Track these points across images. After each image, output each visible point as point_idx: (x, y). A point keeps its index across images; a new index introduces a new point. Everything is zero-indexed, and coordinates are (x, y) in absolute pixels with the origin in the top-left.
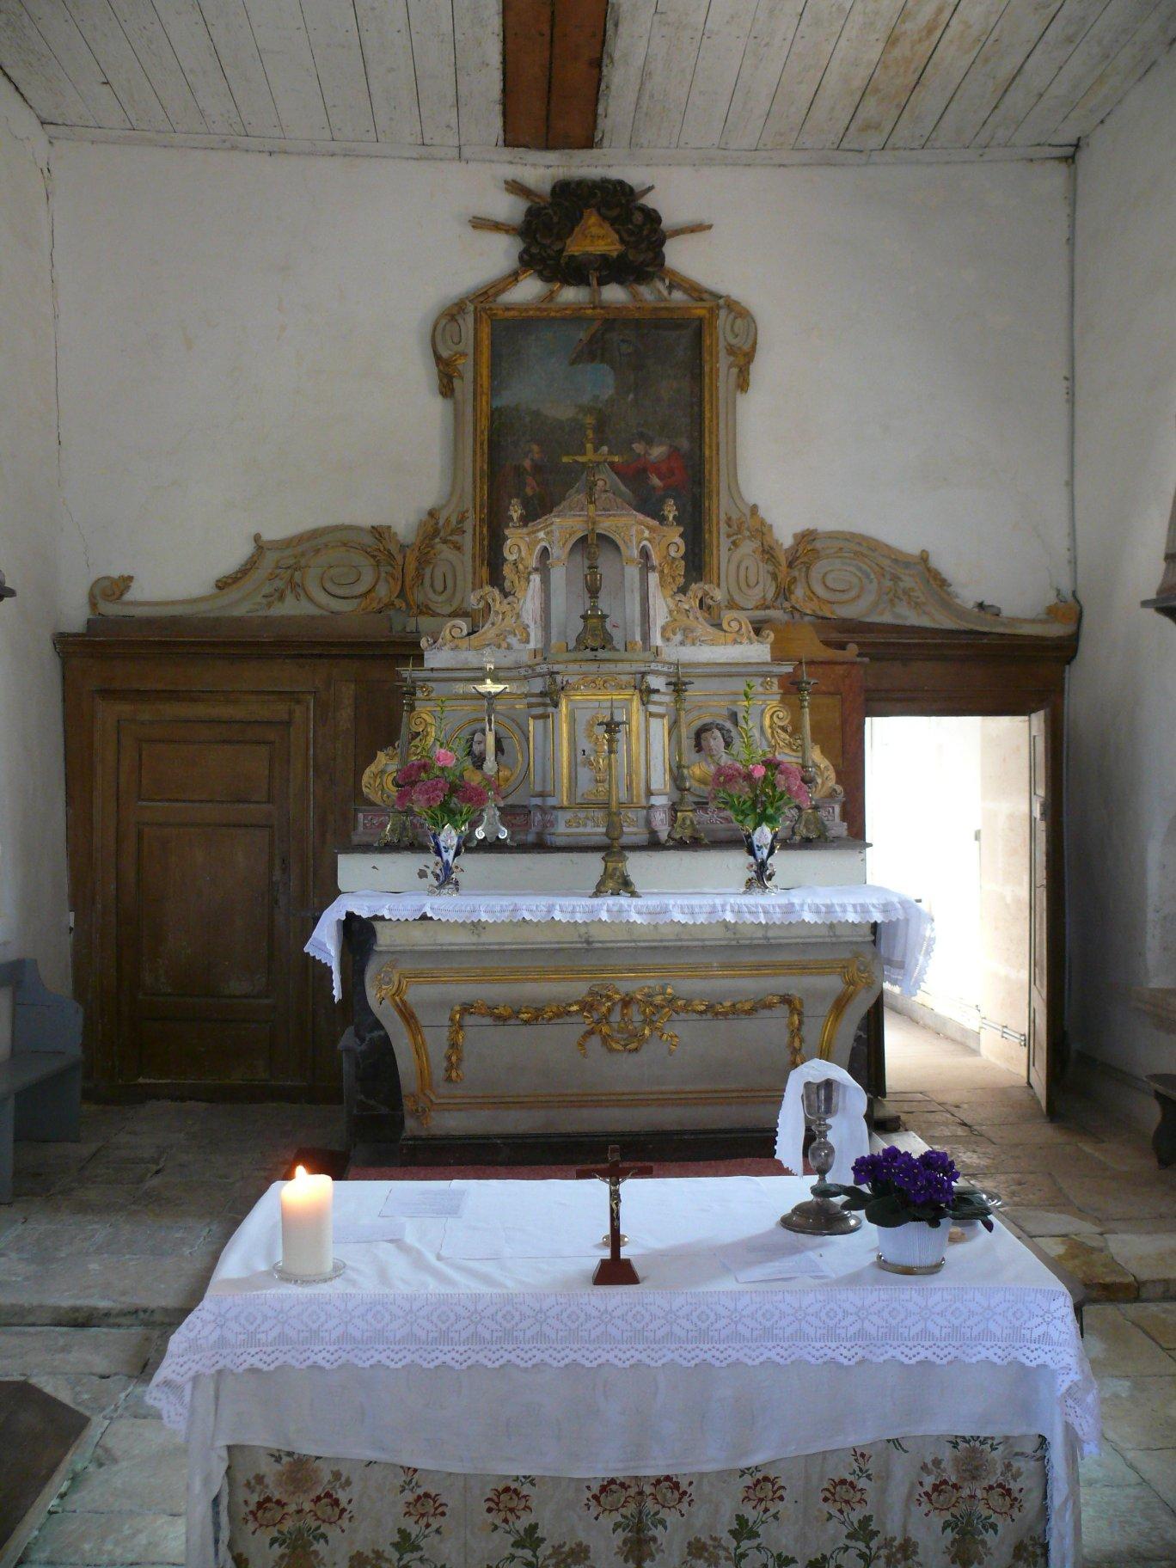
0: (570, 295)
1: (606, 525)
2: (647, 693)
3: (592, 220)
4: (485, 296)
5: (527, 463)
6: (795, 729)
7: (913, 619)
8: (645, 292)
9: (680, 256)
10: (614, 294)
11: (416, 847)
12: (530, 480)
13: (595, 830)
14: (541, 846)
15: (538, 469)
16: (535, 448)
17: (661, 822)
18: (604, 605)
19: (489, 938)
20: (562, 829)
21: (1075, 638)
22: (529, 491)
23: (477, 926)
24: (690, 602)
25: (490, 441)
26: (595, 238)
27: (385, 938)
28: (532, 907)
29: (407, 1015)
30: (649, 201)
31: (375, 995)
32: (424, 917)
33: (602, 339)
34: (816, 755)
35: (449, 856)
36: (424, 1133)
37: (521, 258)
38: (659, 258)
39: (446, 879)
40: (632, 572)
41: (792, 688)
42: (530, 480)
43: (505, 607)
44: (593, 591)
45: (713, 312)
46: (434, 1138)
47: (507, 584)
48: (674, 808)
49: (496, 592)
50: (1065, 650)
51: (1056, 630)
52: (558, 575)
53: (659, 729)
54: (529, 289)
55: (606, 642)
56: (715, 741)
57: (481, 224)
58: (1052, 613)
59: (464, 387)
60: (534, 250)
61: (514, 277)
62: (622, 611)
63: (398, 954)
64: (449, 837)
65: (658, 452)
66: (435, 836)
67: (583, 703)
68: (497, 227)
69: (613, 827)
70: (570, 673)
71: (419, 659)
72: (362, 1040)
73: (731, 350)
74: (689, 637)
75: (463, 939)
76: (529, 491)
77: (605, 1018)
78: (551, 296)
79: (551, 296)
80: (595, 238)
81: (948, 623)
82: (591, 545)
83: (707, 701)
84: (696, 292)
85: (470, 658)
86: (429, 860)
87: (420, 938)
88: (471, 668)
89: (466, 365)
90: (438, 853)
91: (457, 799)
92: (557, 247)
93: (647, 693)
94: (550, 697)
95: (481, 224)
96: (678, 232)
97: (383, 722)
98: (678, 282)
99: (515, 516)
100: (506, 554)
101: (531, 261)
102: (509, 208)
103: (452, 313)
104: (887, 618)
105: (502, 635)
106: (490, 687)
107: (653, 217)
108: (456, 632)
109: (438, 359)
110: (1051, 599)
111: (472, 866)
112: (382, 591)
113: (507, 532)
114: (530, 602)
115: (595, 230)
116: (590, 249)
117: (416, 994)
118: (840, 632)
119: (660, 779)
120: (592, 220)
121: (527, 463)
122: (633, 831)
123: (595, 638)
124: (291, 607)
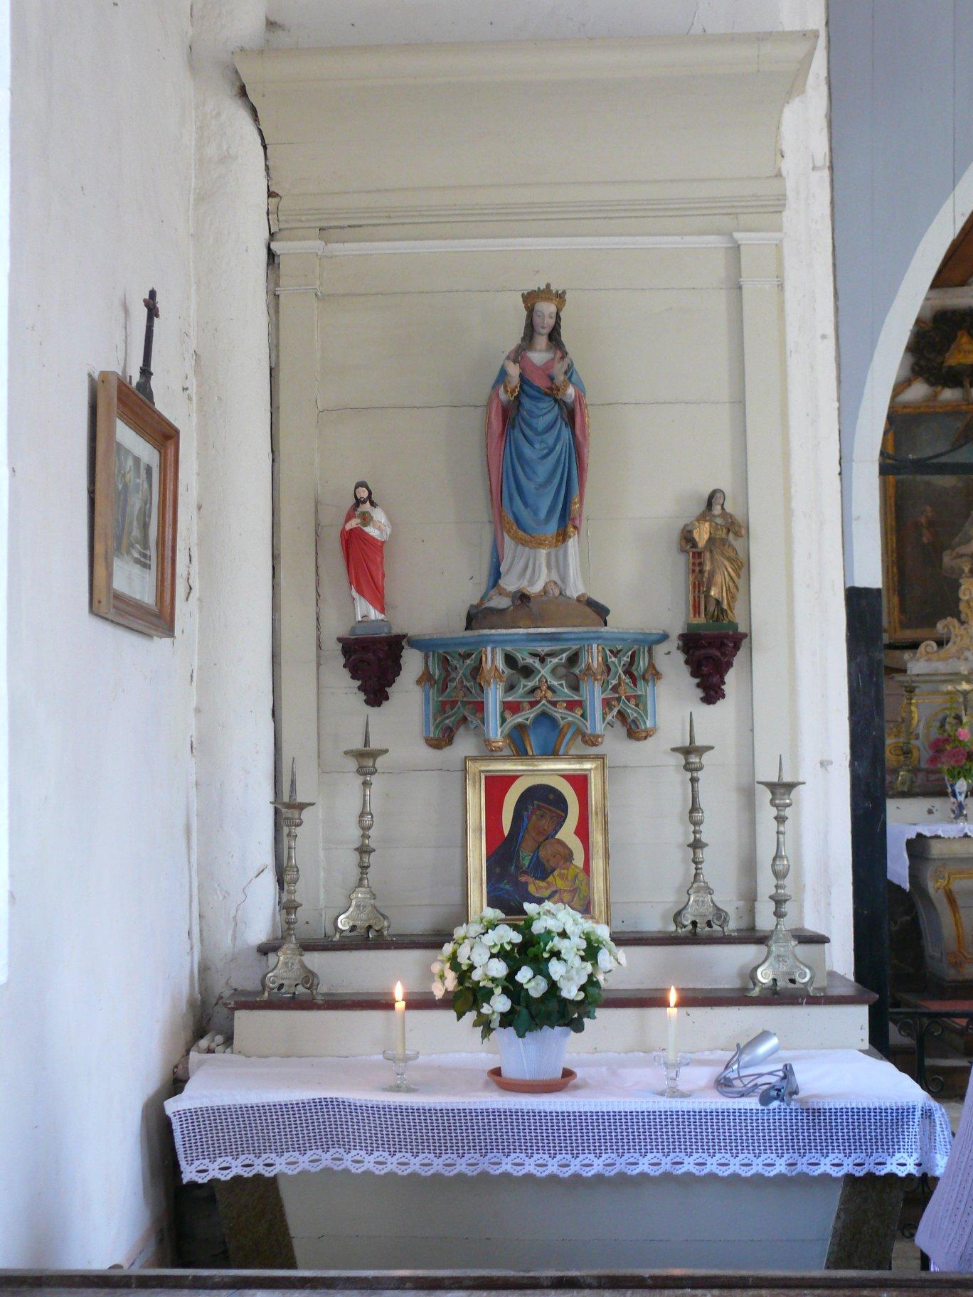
5: (923, 520)
11: (941, 793)
12: (925, 531)
15: (931, 523)
16: (928, 509)
22: (925, 540)
25: (896, 505)
27: (936, 849)
29: (951, 898)
31: (933, 887)
32: (966, 836)
35: (961, 798)
36: (960, 978)
37: (913, 370)
42: (925, 531)
43: (963, 632)
46: (967, 981)
47: (963, 616)
49: (955, 621)
60: (923, 363)
63: (944, 861)
66: (952, 786)
72: (896, 923)
76: (925, 540)
79: (935, 395)
85: (941, 667)
90: (954, 795)
92: (939, 360)
99: (966, 570)
100: (961, 596)
105: (961, 651)
106: (965, 686)
108: (929, 649)
113: (961, 581)
115: (967, 347)
116: (963, 361)
121: (923, 520)
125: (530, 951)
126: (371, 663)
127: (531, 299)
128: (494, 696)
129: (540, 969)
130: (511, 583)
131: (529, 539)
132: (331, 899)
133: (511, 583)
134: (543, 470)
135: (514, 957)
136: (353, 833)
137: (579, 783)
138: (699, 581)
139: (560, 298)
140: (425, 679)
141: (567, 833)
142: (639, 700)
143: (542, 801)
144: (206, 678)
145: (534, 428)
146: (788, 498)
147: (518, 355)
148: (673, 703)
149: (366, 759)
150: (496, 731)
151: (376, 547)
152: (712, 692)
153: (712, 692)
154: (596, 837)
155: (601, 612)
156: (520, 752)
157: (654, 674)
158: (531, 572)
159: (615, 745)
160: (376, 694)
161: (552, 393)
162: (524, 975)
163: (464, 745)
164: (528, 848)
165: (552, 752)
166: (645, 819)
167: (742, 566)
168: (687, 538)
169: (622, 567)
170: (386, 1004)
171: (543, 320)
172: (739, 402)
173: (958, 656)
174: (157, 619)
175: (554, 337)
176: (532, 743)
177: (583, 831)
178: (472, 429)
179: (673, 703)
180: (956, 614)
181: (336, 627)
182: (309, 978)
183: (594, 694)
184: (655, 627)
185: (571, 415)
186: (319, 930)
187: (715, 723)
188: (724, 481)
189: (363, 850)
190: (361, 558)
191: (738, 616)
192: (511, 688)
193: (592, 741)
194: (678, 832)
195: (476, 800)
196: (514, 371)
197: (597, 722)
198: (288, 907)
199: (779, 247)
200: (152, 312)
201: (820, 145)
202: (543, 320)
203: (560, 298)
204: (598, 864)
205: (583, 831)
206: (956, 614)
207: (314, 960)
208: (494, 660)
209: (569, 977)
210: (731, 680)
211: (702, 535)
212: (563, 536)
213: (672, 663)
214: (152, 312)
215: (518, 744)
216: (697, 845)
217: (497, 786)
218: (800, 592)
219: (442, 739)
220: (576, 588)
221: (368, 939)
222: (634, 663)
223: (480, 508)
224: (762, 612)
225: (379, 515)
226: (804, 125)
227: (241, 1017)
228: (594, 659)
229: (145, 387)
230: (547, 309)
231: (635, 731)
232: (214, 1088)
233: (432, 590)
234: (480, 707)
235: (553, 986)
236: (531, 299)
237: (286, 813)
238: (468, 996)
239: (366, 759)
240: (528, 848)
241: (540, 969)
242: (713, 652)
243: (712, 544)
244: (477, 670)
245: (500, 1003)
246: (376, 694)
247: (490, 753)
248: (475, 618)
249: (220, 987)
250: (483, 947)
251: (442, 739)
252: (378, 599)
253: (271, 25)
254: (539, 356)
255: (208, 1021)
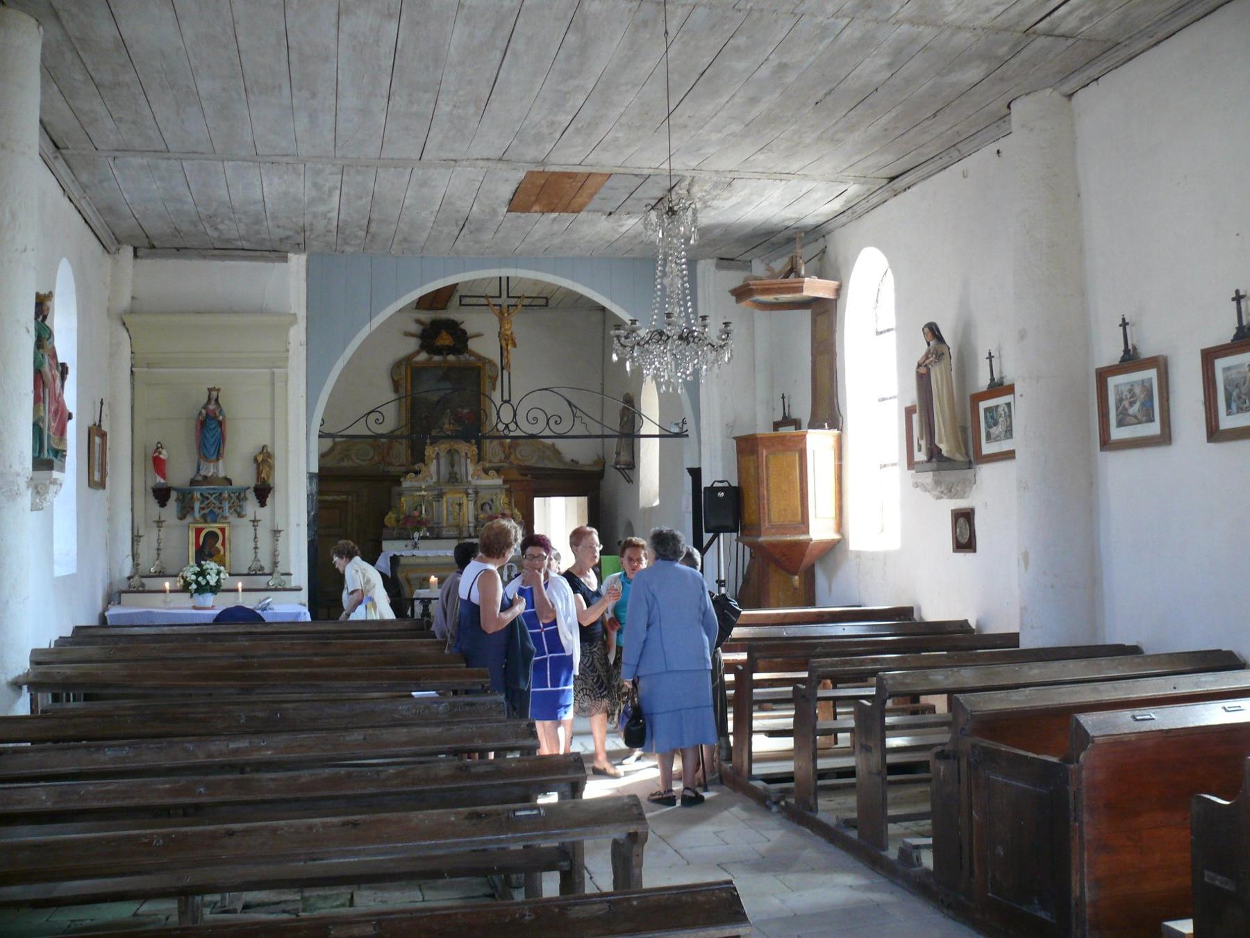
0: (437, 358)
1: (456, 447)
2: (467, 494)
3: (444, 334)
4: (408, 359)
6: (510, 503)
7: (550, 465)
8: (462, 357)
9: (473, 345)
10: (451, 358)
13: (454, 533)
14: (438, 537)
17: (472, 530)
18: (456, 469)
19: (430, 561)
20: (444, 533)
21: (603, 470)
23: (427, 557)
24: (479, 467)
26: (445, 339)
27: (402, 561)
28: (441, 553)
29: (408, 581)
30: (463, 326)
31: (401, 576)
33: (448, 373)
34: (516, 511)
38: (466, 346)
39: (415, 546)
40: (463, 460)
41: (509, 492)
44: (453, 466)
45: (484, 364)
48: (475, 527)
50: (600, 475)
51: (596, 469)
52: (442, 461)
53: (471, 504)
54: (423, 356)
55: (457, 480)
56: (487, 508)
57: (408, 334)
58: (596, 463)
59: (402, 391)
61: (418, 353)
62: (460, 470)
63: (405, 565)
64: (416, 535)
65: (465, 411)
67: (450, 497)
68: (412, 335)
69: (461, 533)
70: (446, 489)
71: (400, 484)
73: (490, 377)
74: (479, 477)
75: (423, 561)
77: (696, 319)
78: (430, 359)
80: (445, 339)
81: (561, 466)
82: (451, 452)
83: (485, 496)
84: (479, 358)
85: (416, 484)
86: (409, 543)
87: (412, 561)
88: (416, 488)
89: (402, 382)
91: (419, 524)
93: (467, 494)
94: (440, 496)
95: (408, 334)
96: (473, 337)
97: (386, 503)
98: (472, 354)
101: (423, 347)
102: (415, 328)
103: (398, 365)
104: (541, 465)
106: (423, 493)
107: (464, 332)
109: (393, 380)
110: (596, 458)
111: (422, 543)
112: (376, 458)
114: (433, 467)
117: (412, 575)
118: (526, 470)
119: (472, 519)
120: (444, 334)
122: (465, 534)
123: (453, 479)
124: (346, 464)
125: (202, 573)
126: (162, 495)
127: (210, 390)
128: (197, 505)
129: (204, 577)
130: (203, 473)
131: (207, 459)
132: (149, 563)
133: (203, 473)
134: (212, 441)
135: (197, 574)
136: (156, 545)
137: (223, 530)
138: (259, 473)
139: (218, 390)
140: (177, 500)
141: (219, 545)
142: (241, 507)
143: (212, 536)
144: (111, 500)
145: (210, 428)
146: (287, 446)
147: (205, 407)
148: (251, 507)
149: (159, 523)
150: (197, 515)
151: (163, 461)
152: (263, 504)
153: (263, 504)
154: (227, 546)
155: (229, 482)
156: (206, 522)
157: (245, 499)
158: (209, 470)
159: (233, 519)
160: (163, 503)
161: (215, 417)
162: (200, 579)
163: (189, 519)
164: (207, 549)
165: (215, 521)
166: (241, 540)
167: (272, 468)
168: (256, 460)
169: (236, 466)
170: (164, 591)
171: (213, 396)
172: (273, 419)
173: (423, 480)
174: (102, 485)
175: (217, 400)
176: (209, 519)
177: (223, 544)
178: (193, 425)
179: (251, 507)
180: (423, 461)
181: (151, 484)
182: (143, 585)
183: (226, 505)
184: (246, 485)
185: (221, 424)
186: (147, 573)
187: (263, 513)
188: (267, 442)
189: (158, 549)
190: (159, 465)
191: (270, 482)
192: (202, 502)
193: (225, 518)
194: (252, 545)
195: (192, 535)
196: (204, 412)
197: (227, 513)
198: (136, 565)
199: (287, 374)
200: (102, 403)
201: (303, 338)
202: (213, 396)
203: (218, 390)
204: (227, 554)
205: (223, 544)
206: (423, 461)
207: (144, 580)
208: (197, 495)
209: (212, 580)
210: (268, 500)
211: (260, 458)
212: (218, 459)
213: (251, 495)
214: (102, 403)
215: (204, 518)
216: (256, 548)
217: (198, 531)
218: (290, 474)
219: (182, 517)
220: (221, 474)
221: (161, 574)
222: (240, 496)
223: (195, 450)
224: (278, 480)
225: (164, 452)
226: (298, 334)
227: (123, 595)
228: (226, 495)
229: (100, 426)
230: (214, 394)
231: (240, 515)
232: (114, 610)
233: (180, 473)
234: (193, 509)
235: (208, 583)
236: (210, 390)
237: (136, 538)
238: (185, 588)
239: (159, 523)
240: (207, 549)
241: (204, 577)
242: (263, 492)
243: (264, 460)
244: (192, 498)
245: (194, 586)
246: (163, 503)
247: (197, 522)
248: (193, 482)
249: (116, 589)
250: (190, 572)
251: (182, 517)
252: (163, 476)
253: (133, 298)
254: (212, 407)
255: (112, 597)
